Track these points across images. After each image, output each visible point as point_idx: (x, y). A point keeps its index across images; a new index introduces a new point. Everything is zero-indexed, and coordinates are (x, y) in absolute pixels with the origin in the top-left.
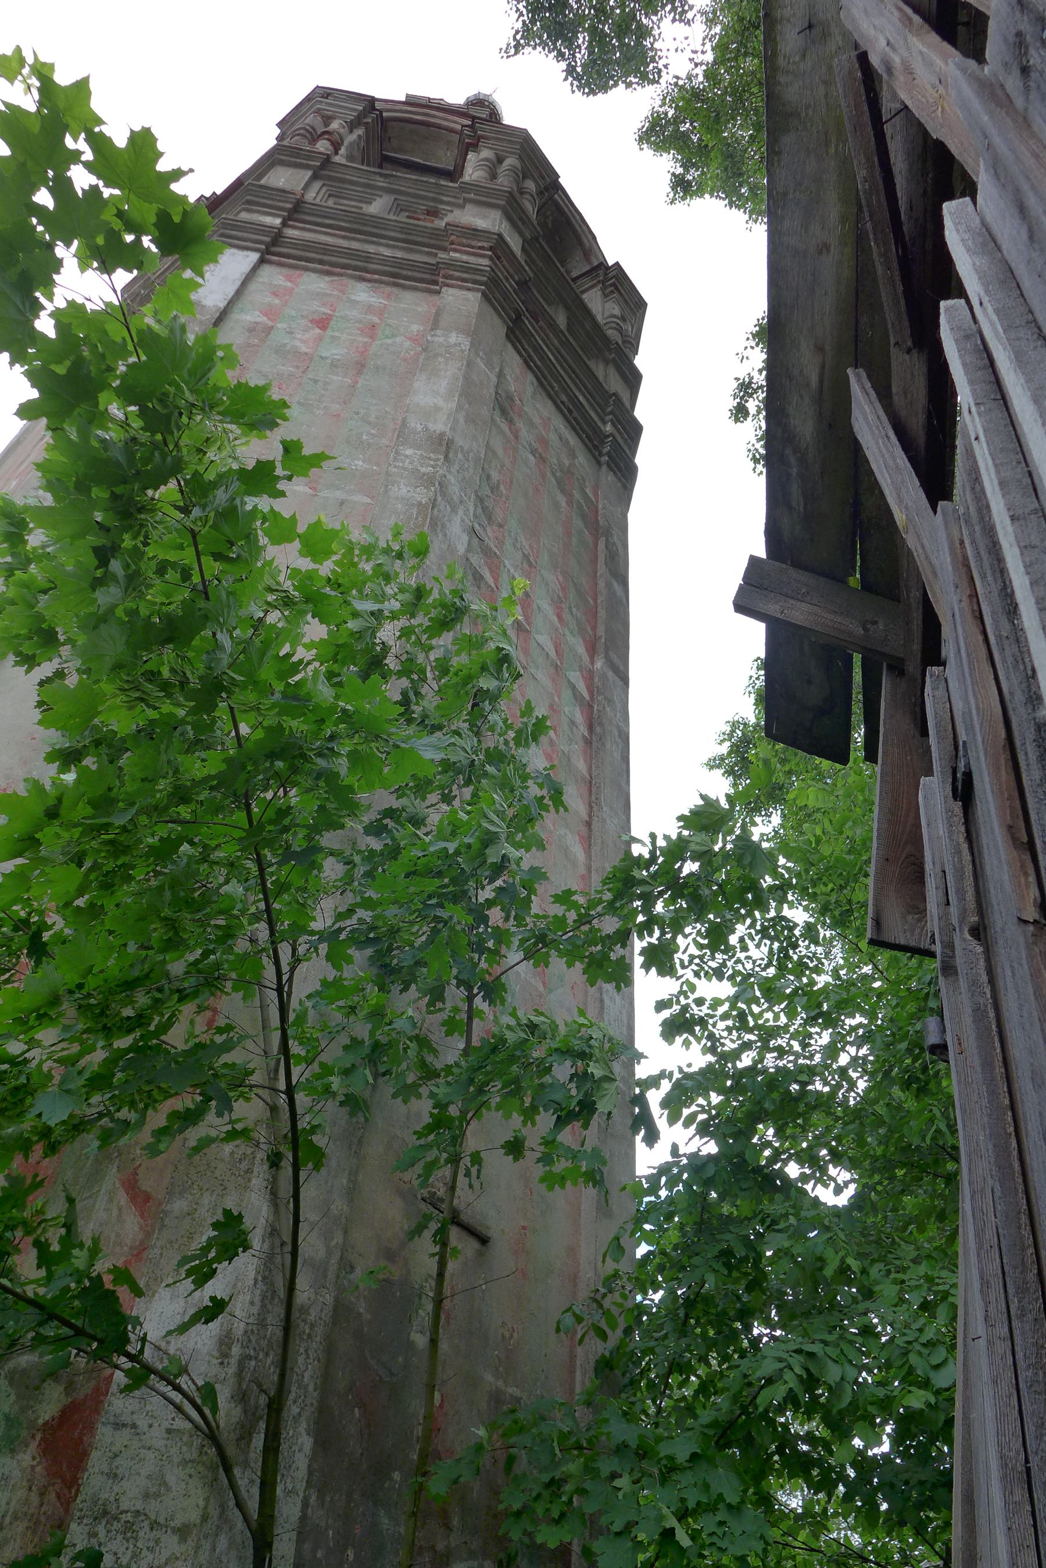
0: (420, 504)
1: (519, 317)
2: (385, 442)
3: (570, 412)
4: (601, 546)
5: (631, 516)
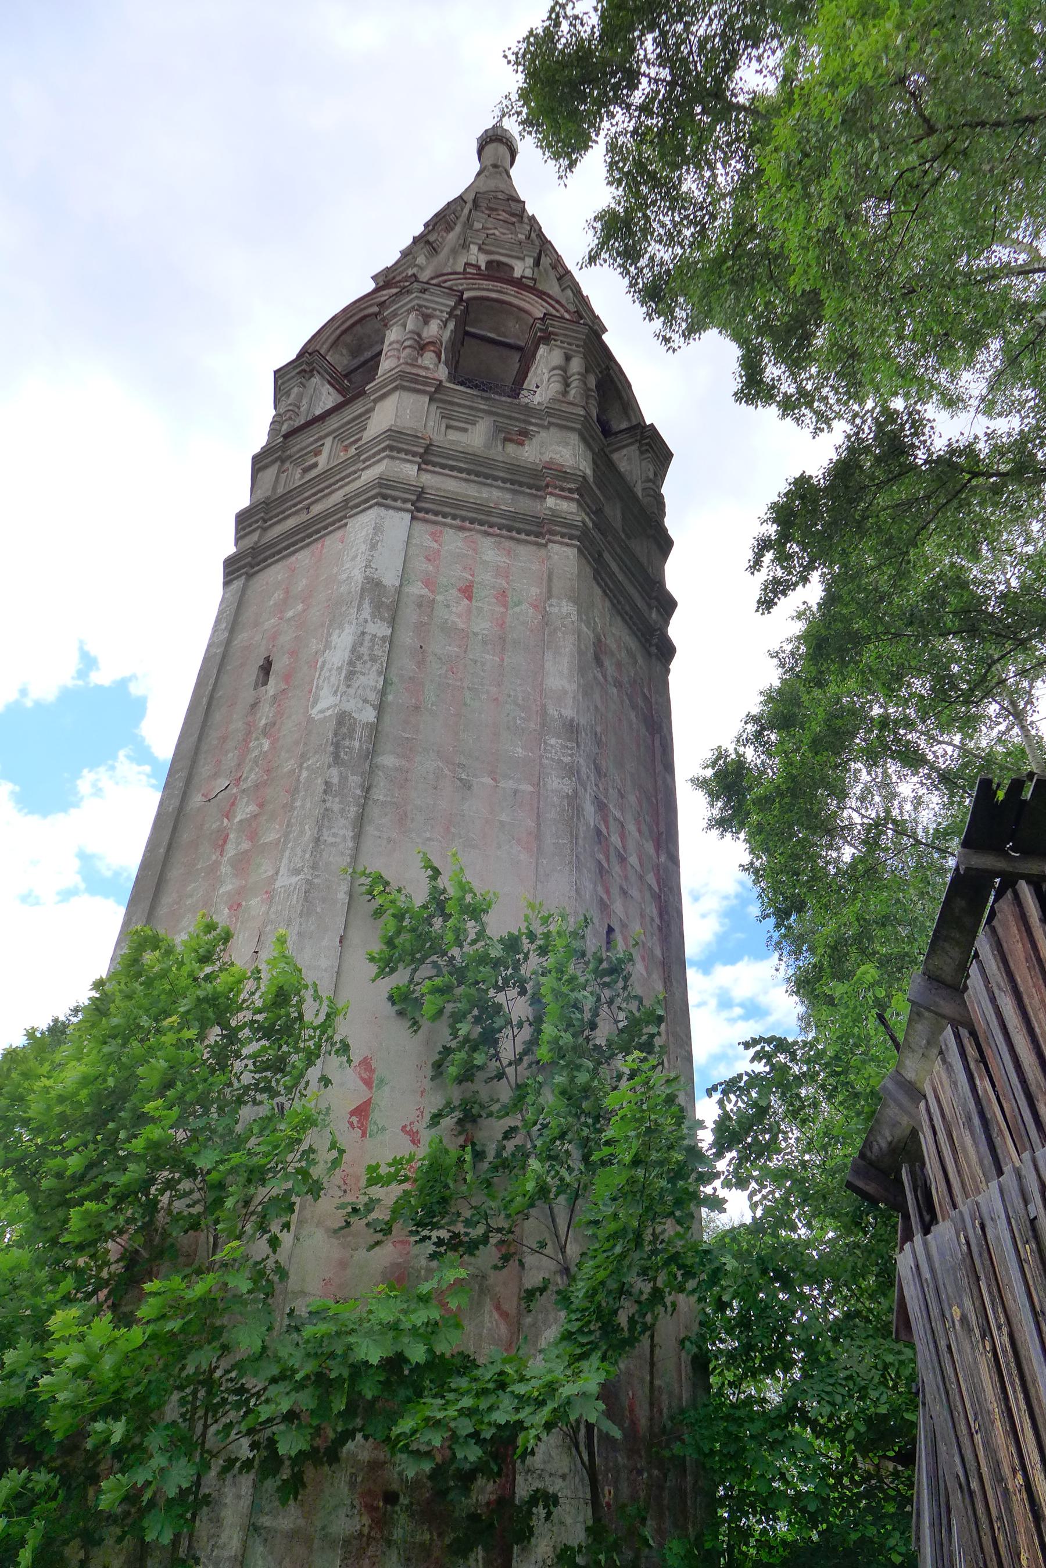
0: (568, 795)
1: (600, 555)
2: (532, 725)
3: (631, 618)
4: (657, 743)
5: (671, 678)
